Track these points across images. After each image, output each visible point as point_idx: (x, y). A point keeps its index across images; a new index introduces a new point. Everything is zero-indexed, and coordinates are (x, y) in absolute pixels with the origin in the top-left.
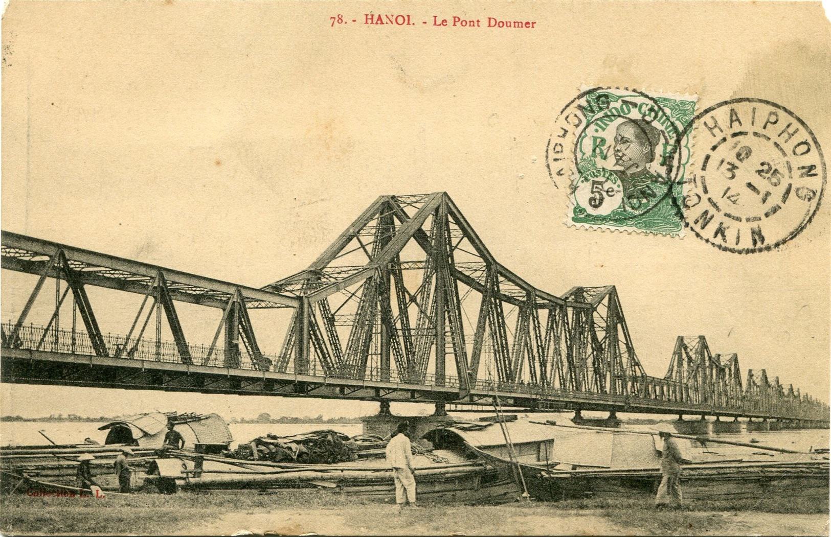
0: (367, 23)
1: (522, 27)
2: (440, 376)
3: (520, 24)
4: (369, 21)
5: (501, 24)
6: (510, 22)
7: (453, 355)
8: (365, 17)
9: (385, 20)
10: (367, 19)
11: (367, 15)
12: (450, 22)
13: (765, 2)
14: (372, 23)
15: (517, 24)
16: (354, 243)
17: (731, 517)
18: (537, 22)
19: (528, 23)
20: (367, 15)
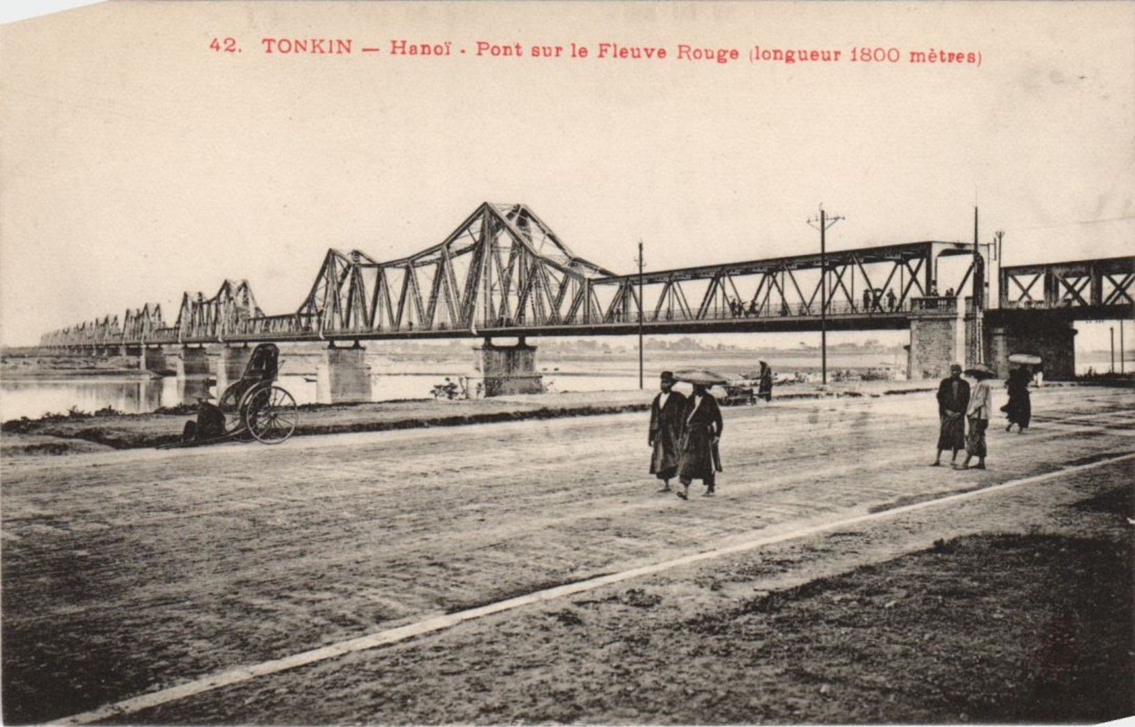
0: (394, 52)
1: (924, 61)
2: (521, 313)
3: (921, 57)
4: (399, 51)
5: (697, 55)
6: (549, 48)
7: (647, 338)
8: (678, 49)
9: (643, 54)
10: (394, 47)
11: (394, 42)
12: (594, 51)
13: (685, 723)
14: (403, 53)
15: (915, 57)
16: (466, 232)
17: (958, 579)
18: (453, 42)
19: (951, 55)
20: (394, 42)
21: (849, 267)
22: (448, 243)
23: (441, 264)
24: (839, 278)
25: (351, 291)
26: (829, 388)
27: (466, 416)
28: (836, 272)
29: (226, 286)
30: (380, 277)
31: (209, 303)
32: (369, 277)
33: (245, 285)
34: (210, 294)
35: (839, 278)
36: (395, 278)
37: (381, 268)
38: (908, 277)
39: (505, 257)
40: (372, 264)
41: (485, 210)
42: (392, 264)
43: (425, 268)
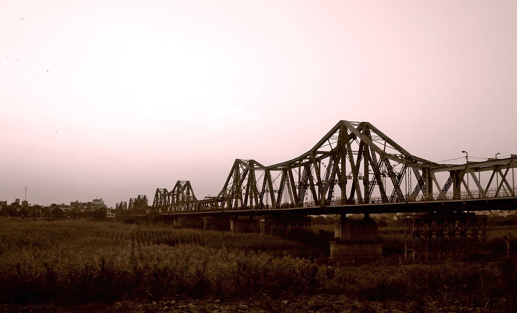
16: (327, 142)
21: (510, 170)
22: (314, 151)
23: (307, 166)
24: (504, 177)
25: (248, 185)
26: (135, 214)
27: (111, 204)
28: (501, 174)
29: (178, 184)
30: (267, 177)
31: (169, 194)
32: (259, 175)
33: (188, 184)
34: (170, 190)
35: (504, 177)
36: (276, 176)
37: (268, 170)
38: (500, 179)
39: (355, 157)
40: (261, 167)
41: (342, 126)
42: (274, 168)
43: (384, 143)
